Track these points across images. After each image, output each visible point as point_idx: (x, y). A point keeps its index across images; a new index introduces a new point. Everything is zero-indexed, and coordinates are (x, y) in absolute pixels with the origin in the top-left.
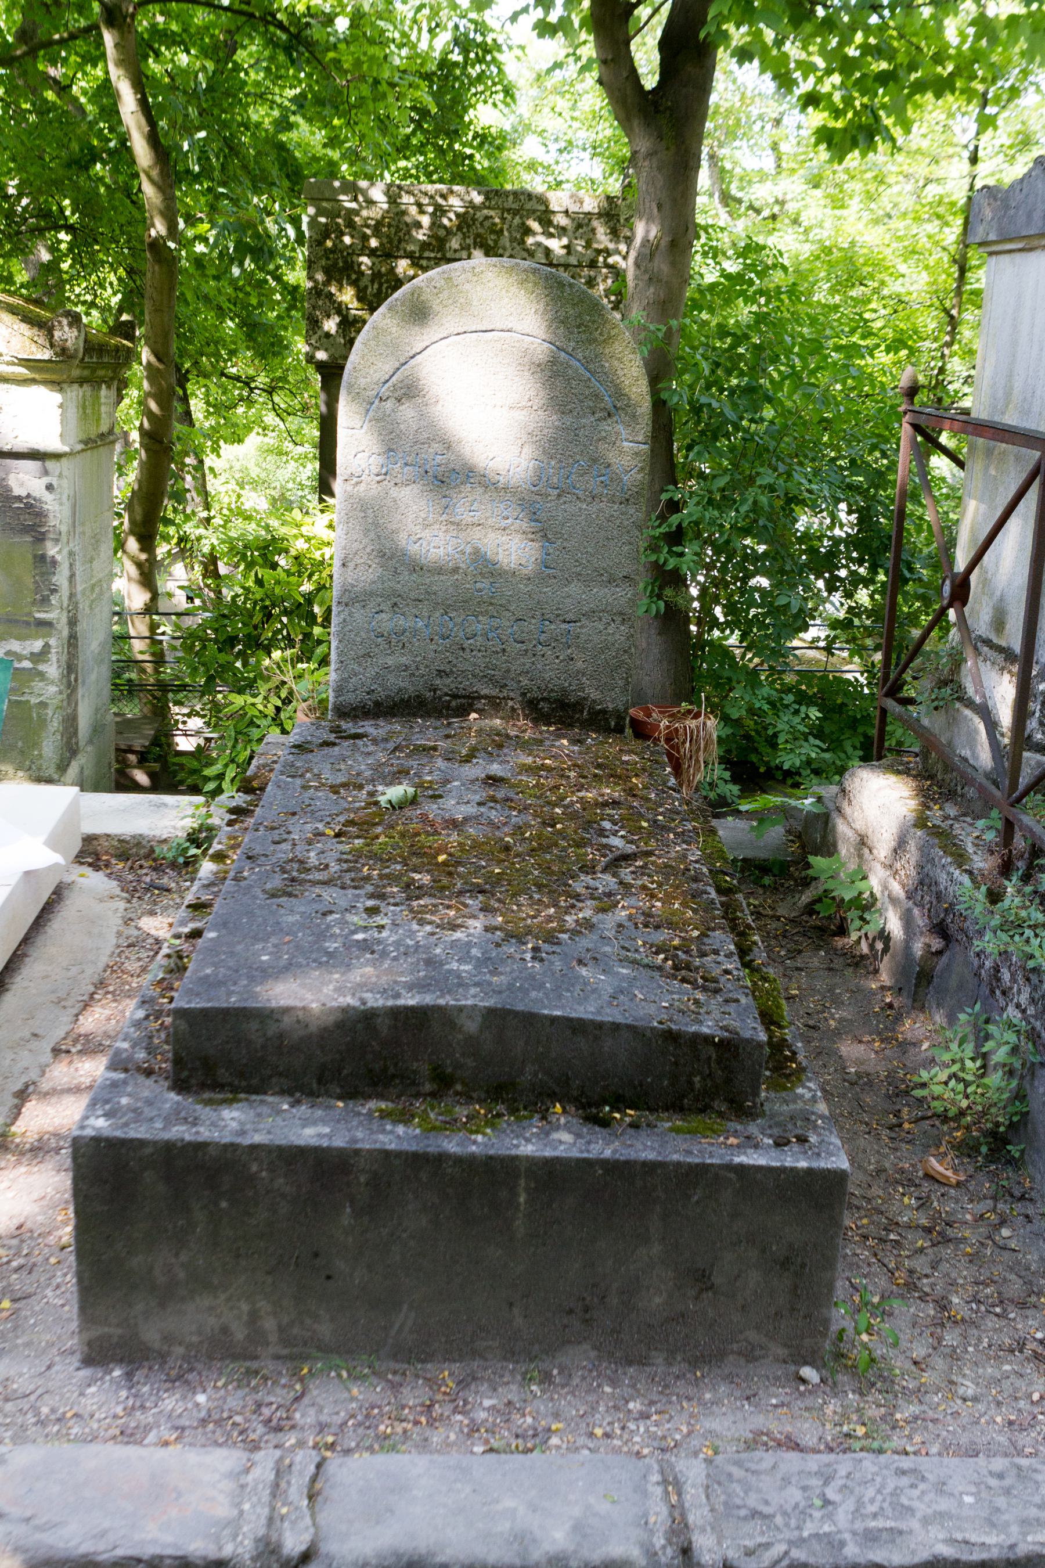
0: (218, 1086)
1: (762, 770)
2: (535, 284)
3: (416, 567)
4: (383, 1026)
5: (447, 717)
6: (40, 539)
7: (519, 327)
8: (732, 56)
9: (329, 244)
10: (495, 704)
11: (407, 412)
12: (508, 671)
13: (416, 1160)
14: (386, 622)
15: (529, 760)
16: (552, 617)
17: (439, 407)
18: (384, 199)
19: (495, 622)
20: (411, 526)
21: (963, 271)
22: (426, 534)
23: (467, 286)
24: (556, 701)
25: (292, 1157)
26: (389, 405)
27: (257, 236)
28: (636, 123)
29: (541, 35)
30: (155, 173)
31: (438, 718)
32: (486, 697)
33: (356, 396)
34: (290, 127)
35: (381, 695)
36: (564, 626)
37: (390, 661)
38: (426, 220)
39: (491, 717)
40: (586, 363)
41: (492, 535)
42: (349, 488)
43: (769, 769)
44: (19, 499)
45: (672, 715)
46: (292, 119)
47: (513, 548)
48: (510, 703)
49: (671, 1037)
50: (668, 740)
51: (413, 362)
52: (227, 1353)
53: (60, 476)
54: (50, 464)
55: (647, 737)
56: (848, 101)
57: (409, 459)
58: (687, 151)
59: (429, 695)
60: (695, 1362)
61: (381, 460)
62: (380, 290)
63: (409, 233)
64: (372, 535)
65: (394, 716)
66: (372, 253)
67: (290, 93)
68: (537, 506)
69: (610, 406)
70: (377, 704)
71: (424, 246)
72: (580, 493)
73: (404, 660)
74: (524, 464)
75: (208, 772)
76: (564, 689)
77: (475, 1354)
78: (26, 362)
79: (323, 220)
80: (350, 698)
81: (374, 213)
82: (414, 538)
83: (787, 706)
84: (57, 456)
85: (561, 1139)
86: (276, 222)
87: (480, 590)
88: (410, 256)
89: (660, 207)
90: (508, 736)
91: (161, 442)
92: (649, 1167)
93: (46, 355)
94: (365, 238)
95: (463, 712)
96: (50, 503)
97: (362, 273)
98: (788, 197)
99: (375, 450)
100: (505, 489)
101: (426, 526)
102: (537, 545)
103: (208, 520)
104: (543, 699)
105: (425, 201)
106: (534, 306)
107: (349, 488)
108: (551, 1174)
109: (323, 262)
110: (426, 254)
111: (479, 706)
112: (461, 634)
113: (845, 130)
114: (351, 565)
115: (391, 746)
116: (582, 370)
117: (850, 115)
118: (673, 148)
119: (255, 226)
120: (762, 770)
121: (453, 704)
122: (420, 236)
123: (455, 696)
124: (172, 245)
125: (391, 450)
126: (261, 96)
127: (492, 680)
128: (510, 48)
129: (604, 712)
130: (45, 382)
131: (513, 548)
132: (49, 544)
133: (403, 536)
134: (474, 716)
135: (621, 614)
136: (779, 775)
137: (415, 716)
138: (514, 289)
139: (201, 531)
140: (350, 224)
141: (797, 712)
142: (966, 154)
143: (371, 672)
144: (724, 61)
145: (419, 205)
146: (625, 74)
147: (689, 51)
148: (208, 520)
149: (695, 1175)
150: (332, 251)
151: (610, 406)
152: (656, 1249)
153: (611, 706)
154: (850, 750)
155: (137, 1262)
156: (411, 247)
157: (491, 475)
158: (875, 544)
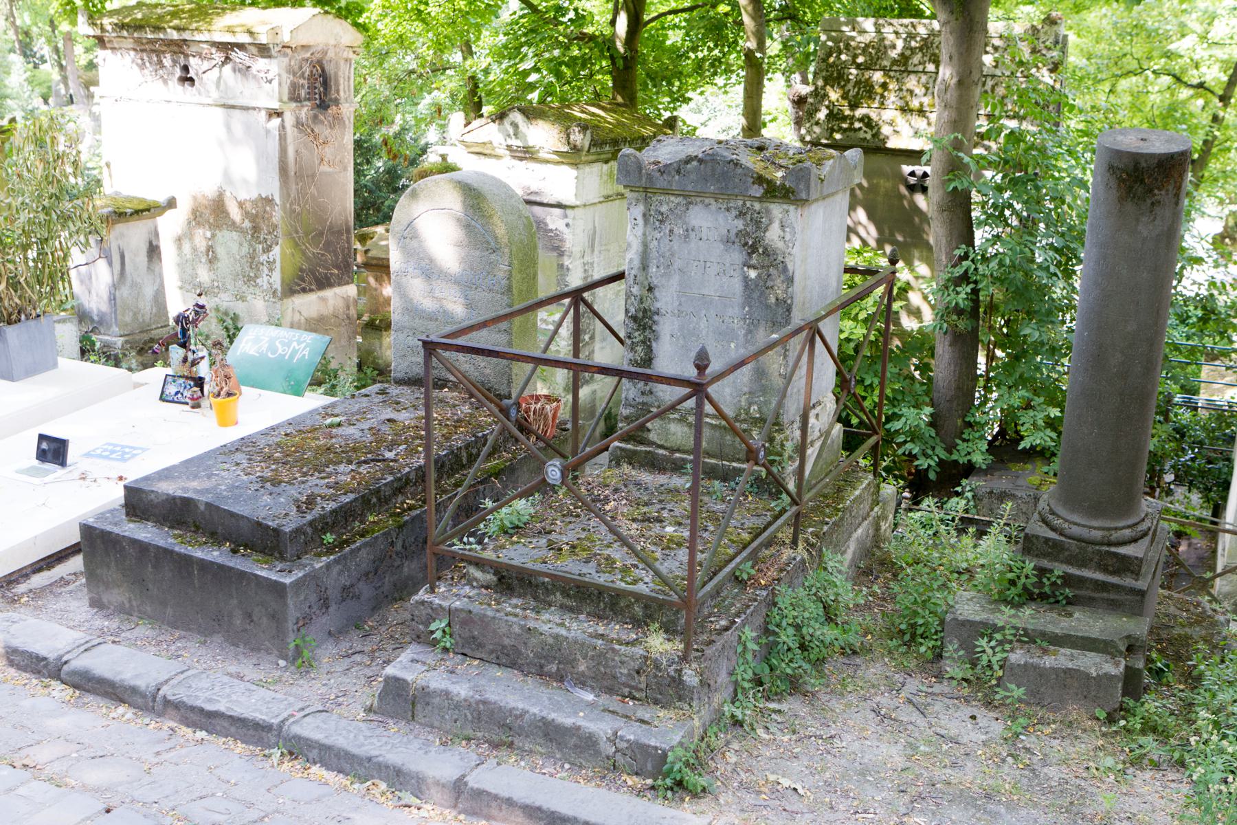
0: (136, 516)
4: (178, 502)
6: (561, 254)
9: (831, 60)
11: (414, 243)
13: (168, 552)
18: (873, 29)
25: (134, 542)
30: (750, 8)
35: (410, 375)
37: (413, 359)
38: (900, 44)
40: (483, 226)
44: (551, 231)
49: (259, 524)
52: (156, 619)
53: (574, 218)
54: (569, 212)
58: (971, 20)
60: (252, 650)
62: (858, 93)
63: (885, 53)
66: (858, 66)
71: (894, 62)
77: (190, 630)
78: (556, 153)
79: (830, 44)
81: (865, 39)
84: (573, 207)
85: (215, 555)
88: (883, 69)
89: (951, 58)
92: (231, 568)
93: (565, 149)
94: (855, 56)
96: (567, 234)
97: (849, 80)
105: (901, 30)
108: (205, 566)
109: (824, 73)
110: (895, 68)
118: (961, 19)
122: (894, 54)
124: (758, 55)
130: (568, 164)
132: (565, 258)
140: (847, 46)
143: (406, 364)
145: (896, 33)
149: (242, 574)
150: (832, 66)
152: (235, 602)
155: (98, 571)
156: (886, 63)
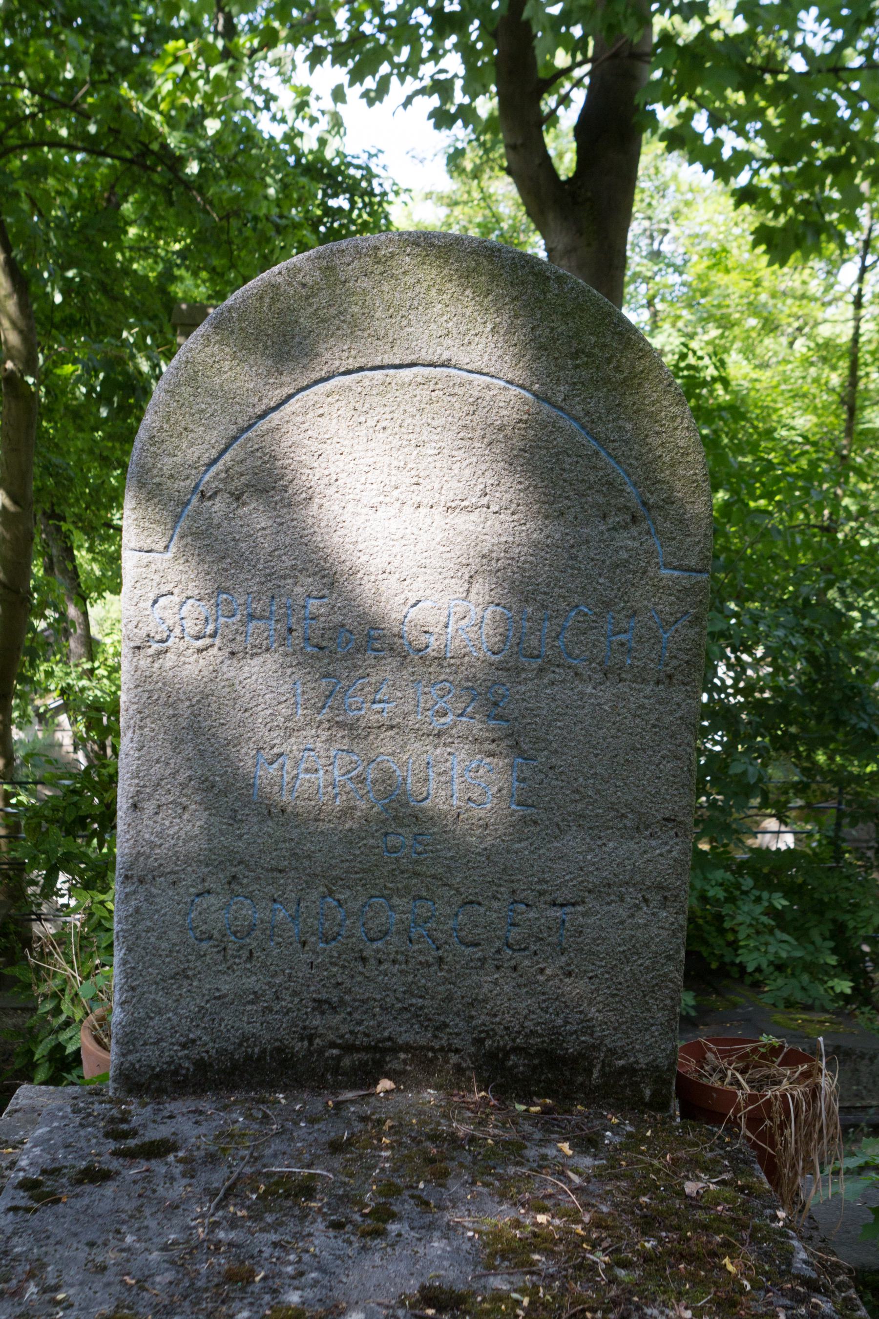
1: (714, 966)
2: (493, 278)
3: (272, 812)
5: (336, 1088)
7: (463, 359)
8: (661, 139)
10: (425, 1062)
12: (449, 998)
14: (218, 911)
15: (502, 1216)
16: (530, 896)
17: (314, 509)
19: (423, 909)
20: (262, 731)
21: (852, 411)
22: (293, 745)
23: (365, 283)
24: (540, 1052)
26: (219, 506)
27: (125, 373)
28: (551, 216)
29: (438, 126)
31: (316, 1091)
32: (407, 1048)
33: (152, 493)
34: (173, 279)
36: (557, 913)
39: (419, 1086)
41: (415, 746)
42: (144, 663)
43: (722, 965)
45: (744, 1057)
46: (177, 272)
47: (460, 779)
48: (454, 1059)
50: (754, 1121)
51: (263, 425)
55: (716, 1117)
56: (787, 196)
57: (257, 607)
59: (300, 1046)
61: (203, 608)
64: (189, 750)
65: (233, 1088)
67: (177, 247)
68: (510, 693)
69: (635, 502)
70: (201, 1065)
72: (581, 666)
73: (250, 982)
74: (475, 613)
75: (44, 989)
76: (554, 1031)
80: (149, 1056)
82: (267, 754)
83: (745, 893)
86: (149, 358)
87: (394, 850)
90: (453, 1138)
91: (17, 592)
95: (366, 1078)
98: (667, 349)
99: (193, 591)
100: (440, 659)
101: (290, 732)
102: (500, 763)
103: (92, 671)
104: (516, 1050)
106: (492, 319)
107: (144, 663)
111: (396, 1065)
112: (360, 932)
113: (784, 229)
114: (149, 807)
115: (218, 1178)
116: (582, 437)
117: (791, 211)
119: (125, 364)
120: (714, 966)
121: (346, 1062)
123: (349, 1048)
125: (220, 590)
126: (146, 250)
127: (417, 1013)
128: (397, 193)
129: (630, 1070)
131: (460, 779)
133: (247, 750)
134: (386, 1084)
135: (660, 887)
136: (735, 972)
137: (273, 1087)
138: (451, 287)
139: (84, 682)
141: (758, 900)
142: (850, 298)
144: (651, 150)
146: (537, 161)
147: (612, 133)
148: (92, 671)
151: (635, 502)
153: (643, 1061)
154: (818, 940)
157: (413, 635)
158: (837, 696)
